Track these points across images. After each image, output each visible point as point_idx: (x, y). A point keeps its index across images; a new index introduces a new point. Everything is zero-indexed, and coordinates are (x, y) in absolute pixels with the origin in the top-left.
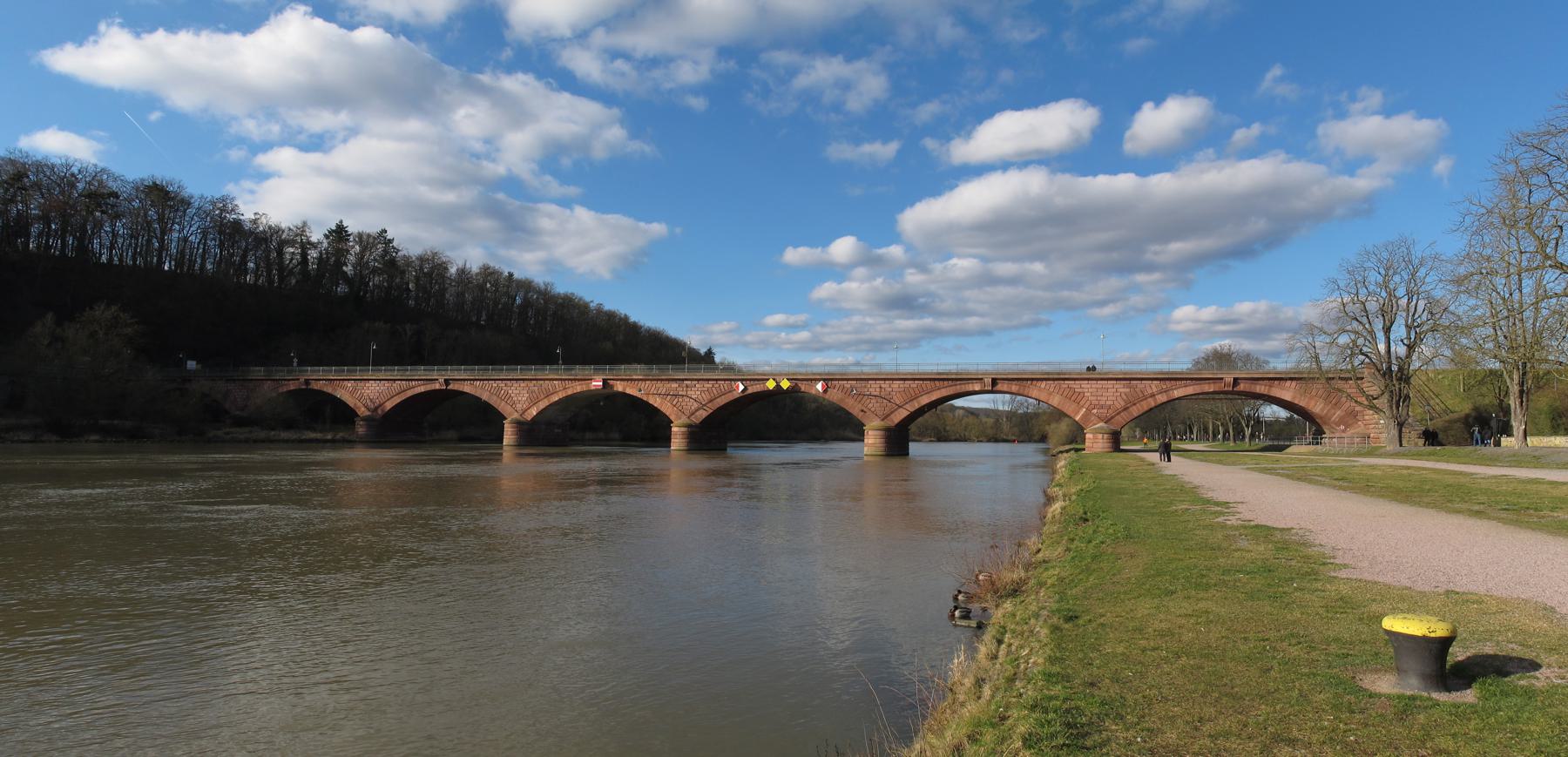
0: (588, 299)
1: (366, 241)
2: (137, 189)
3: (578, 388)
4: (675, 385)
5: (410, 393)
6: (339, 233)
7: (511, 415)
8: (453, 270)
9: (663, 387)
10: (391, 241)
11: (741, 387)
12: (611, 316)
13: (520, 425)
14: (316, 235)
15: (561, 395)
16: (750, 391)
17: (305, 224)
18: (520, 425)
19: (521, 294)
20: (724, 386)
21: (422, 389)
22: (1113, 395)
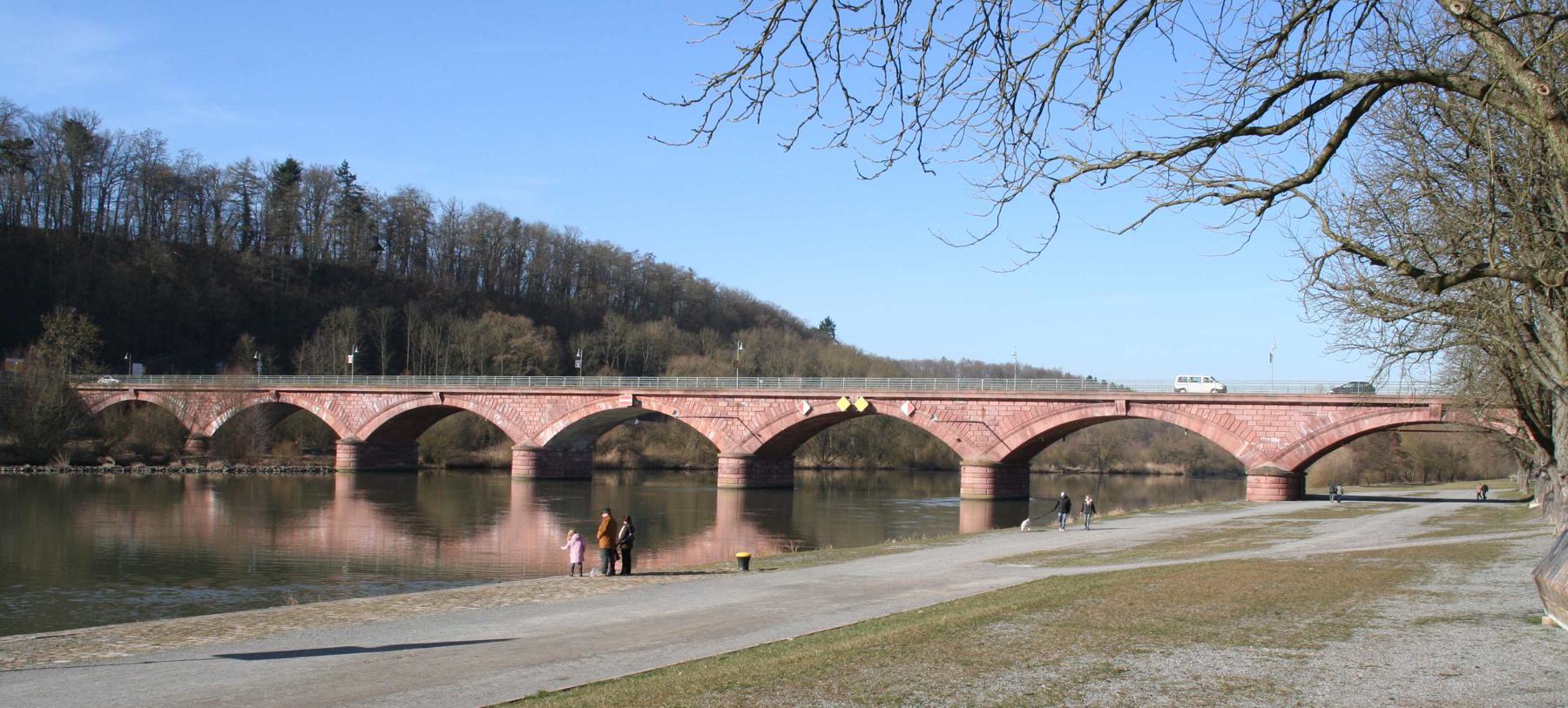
0: (627, 248)
1: (321, 181)
2: (49, 128)
3: (603, 405)
4: (722, 403)
5: (395, 412)
6: (517, 220)
7: (344, 434)
8: (438, 216)
9: (708, 407)
10: (354, 178)
11: (806, 408)
12: (665, 273)
13: (360, 448)
14: (636, 259)
15: (583, 414)
16: (816, 412)
17: (248, 160)
18: (360, 448)
19: (533, 244)
20: (786, 405)
21: (409, 406)
22: (702, 549)
